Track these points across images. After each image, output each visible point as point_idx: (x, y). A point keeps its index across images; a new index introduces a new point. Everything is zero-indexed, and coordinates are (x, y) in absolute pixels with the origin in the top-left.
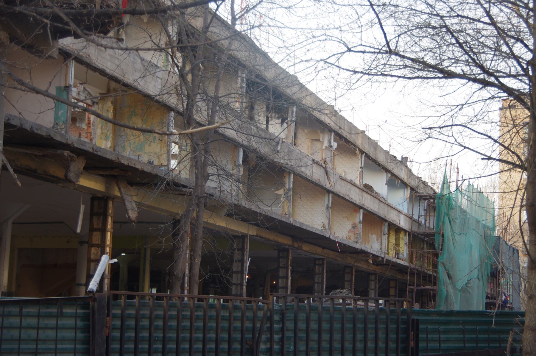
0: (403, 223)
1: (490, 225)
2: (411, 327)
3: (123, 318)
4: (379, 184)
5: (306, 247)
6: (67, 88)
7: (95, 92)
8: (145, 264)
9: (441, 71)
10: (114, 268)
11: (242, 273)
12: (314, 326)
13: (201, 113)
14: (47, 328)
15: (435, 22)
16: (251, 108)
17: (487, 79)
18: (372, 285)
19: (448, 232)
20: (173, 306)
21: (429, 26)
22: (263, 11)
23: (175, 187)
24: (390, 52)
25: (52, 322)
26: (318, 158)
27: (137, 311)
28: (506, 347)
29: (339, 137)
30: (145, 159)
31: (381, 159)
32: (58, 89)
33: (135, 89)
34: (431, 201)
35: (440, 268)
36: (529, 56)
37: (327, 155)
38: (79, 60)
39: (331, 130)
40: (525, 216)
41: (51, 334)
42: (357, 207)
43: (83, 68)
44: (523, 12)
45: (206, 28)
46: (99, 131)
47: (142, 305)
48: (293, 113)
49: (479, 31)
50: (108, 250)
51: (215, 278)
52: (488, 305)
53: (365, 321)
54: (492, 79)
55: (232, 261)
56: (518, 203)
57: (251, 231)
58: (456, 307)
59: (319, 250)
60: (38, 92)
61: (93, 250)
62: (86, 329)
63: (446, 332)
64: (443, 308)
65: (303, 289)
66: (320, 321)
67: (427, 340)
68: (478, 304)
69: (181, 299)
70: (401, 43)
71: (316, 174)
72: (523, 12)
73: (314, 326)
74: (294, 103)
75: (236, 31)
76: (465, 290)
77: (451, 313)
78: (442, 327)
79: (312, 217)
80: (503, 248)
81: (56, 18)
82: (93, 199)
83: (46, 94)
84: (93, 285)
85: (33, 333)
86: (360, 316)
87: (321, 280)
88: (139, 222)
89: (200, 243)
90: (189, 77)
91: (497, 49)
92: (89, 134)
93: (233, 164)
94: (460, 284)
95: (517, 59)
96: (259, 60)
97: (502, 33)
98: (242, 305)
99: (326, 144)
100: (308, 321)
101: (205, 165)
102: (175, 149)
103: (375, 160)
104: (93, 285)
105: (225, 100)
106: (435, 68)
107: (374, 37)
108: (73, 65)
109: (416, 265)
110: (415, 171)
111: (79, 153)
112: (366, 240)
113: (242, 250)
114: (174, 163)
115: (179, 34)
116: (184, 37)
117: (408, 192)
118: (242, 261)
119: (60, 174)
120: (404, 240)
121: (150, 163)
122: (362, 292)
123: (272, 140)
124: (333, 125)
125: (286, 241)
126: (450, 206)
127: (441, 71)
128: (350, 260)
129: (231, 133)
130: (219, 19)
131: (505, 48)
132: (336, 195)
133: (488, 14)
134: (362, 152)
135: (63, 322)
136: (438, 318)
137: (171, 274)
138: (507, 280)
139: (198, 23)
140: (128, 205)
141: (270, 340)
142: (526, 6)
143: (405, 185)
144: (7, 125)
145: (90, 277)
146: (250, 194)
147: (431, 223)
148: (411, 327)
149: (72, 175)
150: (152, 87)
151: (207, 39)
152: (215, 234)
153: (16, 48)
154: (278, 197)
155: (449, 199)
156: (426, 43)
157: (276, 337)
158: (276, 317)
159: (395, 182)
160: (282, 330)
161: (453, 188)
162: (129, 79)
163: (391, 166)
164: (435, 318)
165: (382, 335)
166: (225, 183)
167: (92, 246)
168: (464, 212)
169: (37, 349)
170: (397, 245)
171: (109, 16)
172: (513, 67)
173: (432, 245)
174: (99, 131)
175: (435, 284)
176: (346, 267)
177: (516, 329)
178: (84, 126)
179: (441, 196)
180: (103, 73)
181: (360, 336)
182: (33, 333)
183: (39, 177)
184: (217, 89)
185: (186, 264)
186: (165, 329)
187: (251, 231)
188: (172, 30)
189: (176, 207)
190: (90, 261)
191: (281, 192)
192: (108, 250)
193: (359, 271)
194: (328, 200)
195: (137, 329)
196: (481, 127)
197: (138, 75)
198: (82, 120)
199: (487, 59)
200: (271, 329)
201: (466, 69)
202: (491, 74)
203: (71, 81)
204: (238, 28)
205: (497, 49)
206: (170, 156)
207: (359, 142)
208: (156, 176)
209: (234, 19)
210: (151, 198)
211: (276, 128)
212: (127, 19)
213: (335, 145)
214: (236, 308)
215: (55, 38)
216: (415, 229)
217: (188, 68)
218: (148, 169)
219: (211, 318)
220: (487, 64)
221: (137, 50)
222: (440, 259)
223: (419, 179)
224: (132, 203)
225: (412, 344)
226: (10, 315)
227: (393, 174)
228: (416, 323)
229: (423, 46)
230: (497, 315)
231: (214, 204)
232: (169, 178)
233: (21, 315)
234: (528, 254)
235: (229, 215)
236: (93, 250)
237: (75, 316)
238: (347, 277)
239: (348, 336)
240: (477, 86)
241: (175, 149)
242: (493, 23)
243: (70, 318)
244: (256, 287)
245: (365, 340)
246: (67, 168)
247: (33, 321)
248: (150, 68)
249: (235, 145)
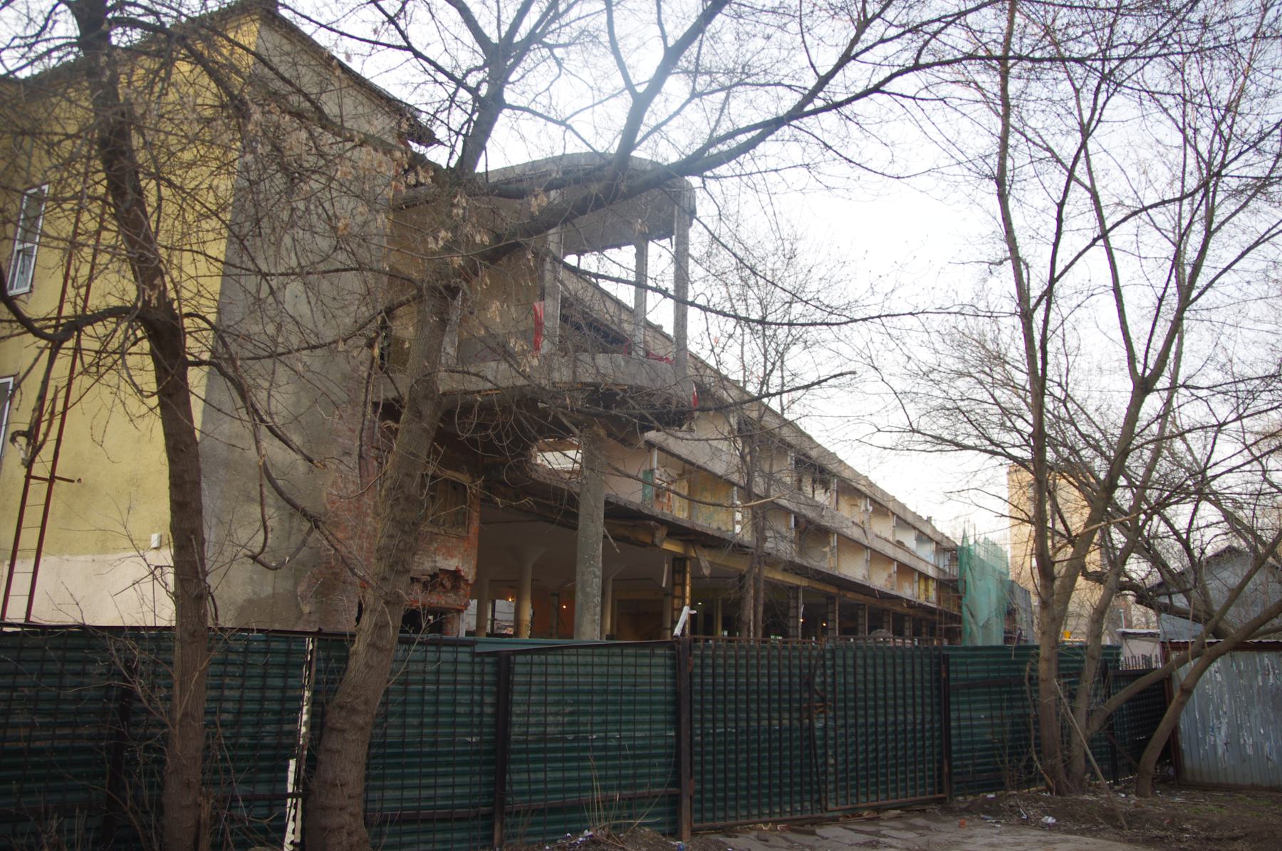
0: (931, 572)
1: (1004, 570)
2: (942, 661)
3: (702, 657)
4: (909, 540)
5: (850, 595)
6: (652, 471)
7: (674, 473)
8: (718, 611)
9: (957, 445)
10: (692, 616)
11: (797, 618)
12: (860, 662)
13: (759, 487)
14: (642, 665)
15: (949, 405)
16: (800, 481)
17: (996, 449)
18: (907, 625)
19: (969, 578)
20: (742, 647)
21: (944, 408)
22: (807, 402)
23: (740, 548)
24: (913, 431)
25: (647, 661)
26: (857, 520)
27: (714, 652)
29: (874, 501)
30: (714, 526)
31: (910, 519)
32: (645, 472)
33: (706, 470)
34: (954, 552)
35: (964, 609)
36: (1030, 430)
37: (865, 517)
38: (661, 449)
39: (866, 496)
40: (1034, 563)
41: (646, 670)
42: (891, 560)
43: (664, 455)
44: (1021, 393)
45: (761, 417)
46: (677, 504)
47: (717, 647)
48: (834, 486)
49: (986, 411)
50: (687, 601)
51: (775, 621)
52: (1006, 640)
53: (894, 657)
54: (999, 450)
55: (789, 608)
56: (1029, 552)
57: (804, 583)
58: (979, 643)
59: (861, 597)
60: (629, 477)
61: (676, 601)
62: (673, 667)
63: (972, 664)
64: (968, 643)
65: (849, 630)
66: (865, 658)
67: (956, 672)
68: (997, 640)
69: (748, 641)
70: (922, 423)
71: (855, 533)
72: (1021, 393)
73: (860, 662)
74: (834, 475)
75: (785, 420)
76: (986, 626)
77: (976, 648)
78: (969, 660)
79: (854, 569)
80: (1017, 591)
81: (642, 418)
82: (674, 560)
83: (637, 479)
84: (677, 631)
85: (632, 670)
86: (899, 653)
87: (864, 622)
88: (712, 577)
89: (762, 595)
90: (748, 458)
91: (1003, 425)
92: (669, 507)
93: (786, 528)
94: (981, 624)
95: (1019, 431)
96: (806, 444)
97: (1005, 411)
98: (799, 646)
99: (863, 508)
100: (855, 658)
101: (764, 529)
102: (738, 516)
103: (904, 521)
104: (677, 631)
105: (778, 476)
106: (952, 442)
107: (899, 419)
108: (656, 453)
109: (943, 607)
110: (939, 529)
111: (663, 522)
112: (901, 587)
113: (797, 598)
114: (738, 528)
115: (739, 424)
116: (743, 426)
117: (934, 545)
118: (797, 608)
119: (648, 540)
120: (932, 586)
121: (719, 529)
122: (899, 632)
123: (818, 507)
124: (868, 492)
125: (831, 590)
126: (969, 556)
127: (957, 445)
128: (887, 605)
129: (783, 502)
130: (771, 410)
131: (1009, 424)
132: (873, 550)
133: (993, 396)
134: (894, 514)
135: (655, 661)
137: (739, 619)
138: (1022, 616)
139: (754, 415)
140: (703, 564)
141: (824, 674)
142: (1024, 389)
143: (931, 540)
144: (607, 503)
145: (675, 623)
146: (802, 551)
147: (955, 571)
148: (942, 661)
149: (657, 541)
150: (719, 468)
151: (762, 428)
152: (773, 586)
153: (612, 442)
154: (825, 553)
155: (969, 550)
156: (943, 422)
157: (829, 672)
158: (828, 656)
159: (923, 537)
160: (833, 666)
161: (971, 542)
162: (701, 462)
163: (918, 525)
164: (962, 652)
165: (917, 668)
166: (781, 544)
167: (674, 597)
168: (982, 560)
170: (927, 590)
171: (684, 414)
172: (1014, 438)
173: (956, 590)
174: (677, 504)
175: (960, 622)
176: (884, 610)
177: (1033, 660)
178: (665, 500)
179: (962, 548)
180: (679, 457)
181: (899, 670)
182: (632, 670)
183: (632, 543)
184: (771, 466)
185: (751, 613)
186: (736, 666)
187: (804, 583)
188: (733, 421)
189: (741, 565)
190: (673, 610)
191: (827, 549)
192: (687, 601)
193: (895, 613)
194: (867, 555)
195: (714, 667)
196: (992, 490)
197: (707, 458)
198: (664, 496)
199: (996, 434)
200: (824, 666)
201: (978, 442)
202: (998, 446)
203: (655, 465)
204: (786, 416)
205: (1003, 425)
206: (735, 522)
207: (890, 505)
208: (724, 540)
209: (783, 409)
210: (722, 559)
211: (821, 497)
212: (697, 414)
213: (871, 509)
214: (794, 648)
215: (642, 432)
216: (941, 577)
217: (747, 450)
218: (717, 534)
219: (774, 657)
220: (995, 437)
221: (707, 440)
222: (965, 601)
223: (943, 534)
224: (706, 562)
225: (944, 675)
226: (613, 655)
227: (921, 532)
228: (947, 658)
229: (940, 425)
230: (1016, 649)
231: (771, 561)
232: (735, 541)
233: (622, 655)
234: (1039, 594)
235: (785, 570)
236: (676, 601)
237: (665, 656)
238: (885, 619)
239: (889, 670)
240: (987, 456)
241: (738, 516)
242: (998, 404)
243: (661, 658)
244: (810, 628)
245: (904, 672)
246: (653, 535)
247: (632, 660)
248: (716, 452)
249: (787, 511)
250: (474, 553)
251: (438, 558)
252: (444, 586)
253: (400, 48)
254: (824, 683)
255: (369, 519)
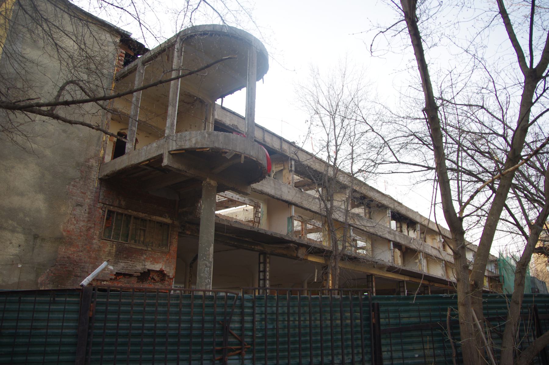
5: (436, 285)
28: (446, 321)
38: (296, 205)
57: (407, 279)
78: (402, 308)
80: (537, 282)
99: (438, 240)
108: (293, 208)
136: (398, 302)
144: (216, 223)
147: (498, 273)
169: (32, 326)
173: (499, 281)
191: (417, 261)
211: (412, 234)
213: (443, 240)
222: (504, 287)
250: (174, 261)
251: (146, 263)
252: (154, 280)
253: (395, 162)
254: (241, 329)
255: (95, 241)
